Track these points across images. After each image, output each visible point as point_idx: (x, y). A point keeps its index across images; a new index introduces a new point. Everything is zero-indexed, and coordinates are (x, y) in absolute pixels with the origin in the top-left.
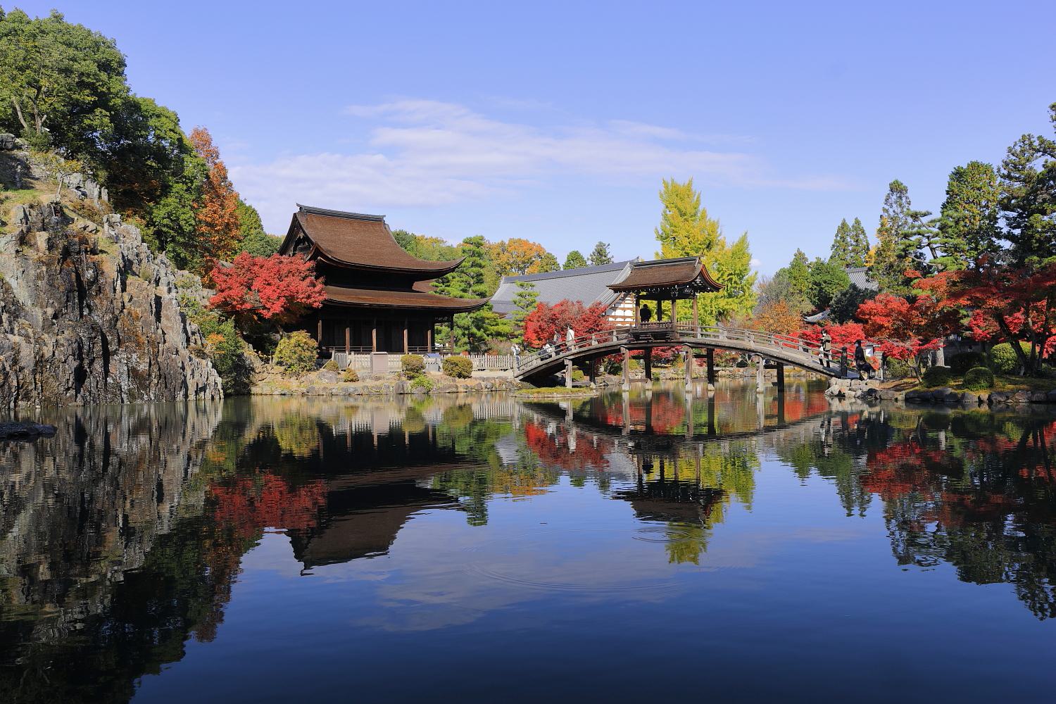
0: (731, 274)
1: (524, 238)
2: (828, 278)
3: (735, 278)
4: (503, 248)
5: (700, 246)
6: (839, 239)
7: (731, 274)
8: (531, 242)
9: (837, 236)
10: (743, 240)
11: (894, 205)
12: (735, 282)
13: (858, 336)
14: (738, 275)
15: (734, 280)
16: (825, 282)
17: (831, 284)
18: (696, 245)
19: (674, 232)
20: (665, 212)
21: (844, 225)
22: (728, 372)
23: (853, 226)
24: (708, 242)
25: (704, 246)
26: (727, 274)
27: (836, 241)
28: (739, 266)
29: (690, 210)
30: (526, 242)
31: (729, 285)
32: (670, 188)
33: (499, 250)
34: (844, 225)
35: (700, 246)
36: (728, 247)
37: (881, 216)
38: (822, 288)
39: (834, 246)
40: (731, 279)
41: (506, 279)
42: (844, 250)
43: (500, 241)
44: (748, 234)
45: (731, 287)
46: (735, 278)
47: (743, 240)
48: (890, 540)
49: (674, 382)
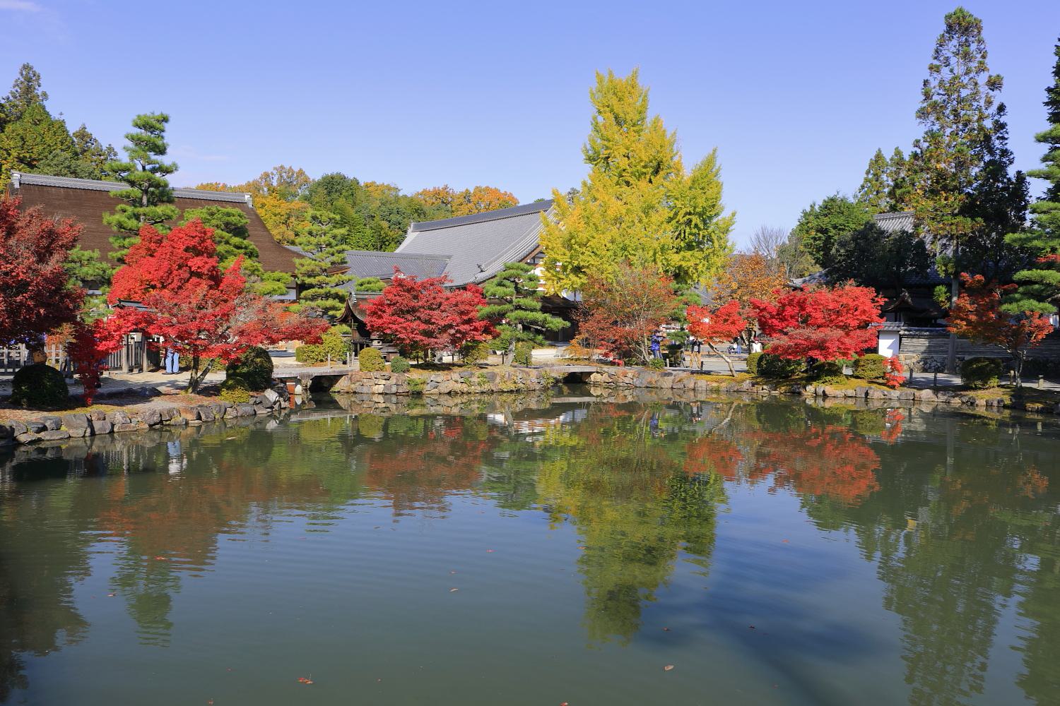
0: (690, 214)
1: (492, 186)
2: (840, 220)
3: (695, 220)
4: (467, 196)
5: (644, 170)
6: (870, 176)
7: (690, 214)
8: (502, 191)
9: (868, 173)
10: (710, 162)
11: (953, 60)
12: (696, 225)
13: (864, 312)
14: (700, 215)
15: (693, 223)
16: (835, 227)
17: (843, 230)
18: (639, 167)
19: (607, 148)
20: (595, 118)
21: (879, 156)
22: (605, 378)
23: (891, 160)
24: (655, 163)
25: (651, 170)
26: (682, 212)
27: (867, 180)
28: (701, 202)
29: (632, 116)
30: (497, 191)
31: (688, 230)
32: (606, 83)
33: (462, 200)
34: (879, 156)
35: (644, 170)
36: (687, 173)
37: (926, 83)
38: (830, 237)
39: (863, 187)
40: (690, 221)
41: (415, 225)
42: (878, 192)
43: (464, 190)
44: (718, 152)
45: (690, 234)
46: (695, 220)
47: (710, 162)
48: (994, 69)
49: (458, 400)
